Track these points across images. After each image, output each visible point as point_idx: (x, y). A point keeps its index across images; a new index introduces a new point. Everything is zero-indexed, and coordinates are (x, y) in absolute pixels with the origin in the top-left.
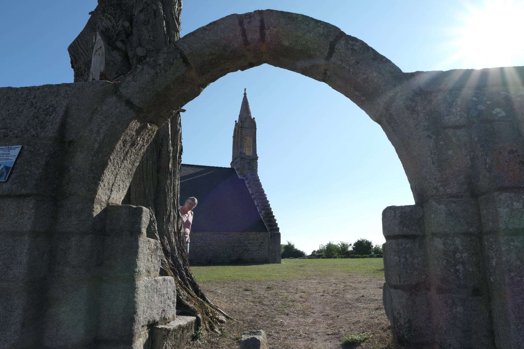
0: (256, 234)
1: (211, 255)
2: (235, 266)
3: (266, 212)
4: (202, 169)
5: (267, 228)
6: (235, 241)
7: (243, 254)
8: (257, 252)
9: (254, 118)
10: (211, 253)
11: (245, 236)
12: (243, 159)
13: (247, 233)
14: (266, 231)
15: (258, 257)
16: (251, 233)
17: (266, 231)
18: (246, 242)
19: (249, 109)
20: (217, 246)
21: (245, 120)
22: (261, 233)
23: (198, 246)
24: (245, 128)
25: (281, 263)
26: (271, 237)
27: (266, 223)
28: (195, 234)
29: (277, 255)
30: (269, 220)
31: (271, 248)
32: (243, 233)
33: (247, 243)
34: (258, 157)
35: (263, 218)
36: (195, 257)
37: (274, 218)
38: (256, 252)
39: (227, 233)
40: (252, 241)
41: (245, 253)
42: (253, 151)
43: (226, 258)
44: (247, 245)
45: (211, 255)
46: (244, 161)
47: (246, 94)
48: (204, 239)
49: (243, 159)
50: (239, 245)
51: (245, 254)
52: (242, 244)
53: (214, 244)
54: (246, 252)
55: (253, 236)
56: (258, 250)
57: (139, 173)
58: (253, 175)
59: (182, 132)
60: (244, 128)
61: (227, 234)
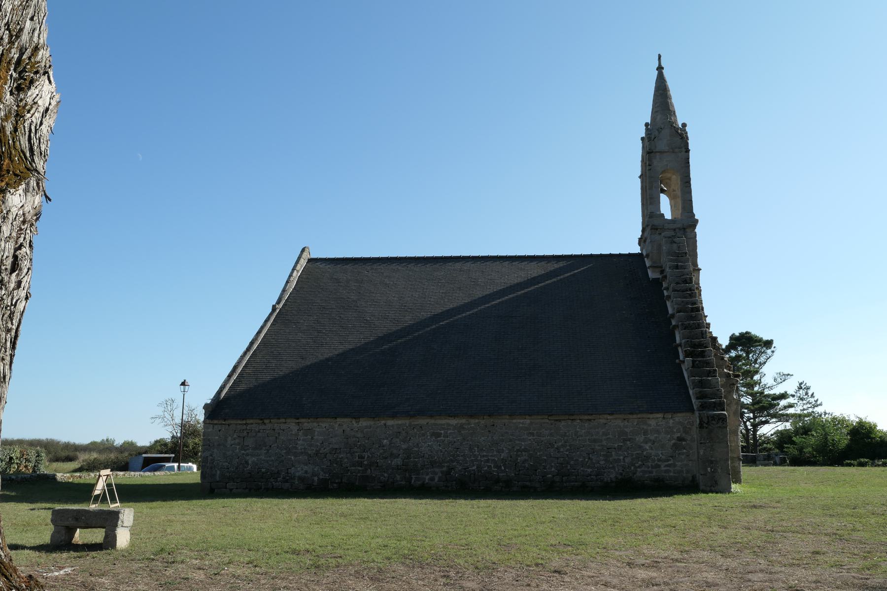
0: (664, 418)
1: (553, 469)
2: (415, 498)
3: (696, 361)
4: (562, 264)
5: (693, 401)
6: (610, 436)
7: (632, 468)
8: (670, 462)
9: (684, 125)
10: (553, 464)
11: (635, 424)
12: (657, 229)
13: (639, 416)
14: (692, 410)
15: (671, 474)
16: (651, 416)
17: (692, 410)
18: (640, 439)
19: (671, 103)
20: (568, 447)
21: (659, 132)
22: (679, 415)
23: (523, 447)
25: (730, 492)
26: (701, 426)
27: (694, 388)
28: (514, 421)
29: (719, 470)
30: (700, 381)
31: (702, 453)
32: (631, 416)
34: (697, 221)
35: (688, 376)
36: (515, 474)
38: (667, 463)
39: (590, 417)
40: (655, 435)
41: (637, 465)
42: (684, 208)
43: (590, 475)
44: (642, 444)
45: (553, 469)
46: (660, 234)
47: (663, 68)
48: (535, 432)
50: (621, 446)
51: (639, 467)
52: (628, 442)
53: (560, 444)
54: (640, 463)
55: (657, 423)
56: (672, 457)
58: (677, 267)
59: (25, 311)
60: (656, 152)
61: (590, 420)
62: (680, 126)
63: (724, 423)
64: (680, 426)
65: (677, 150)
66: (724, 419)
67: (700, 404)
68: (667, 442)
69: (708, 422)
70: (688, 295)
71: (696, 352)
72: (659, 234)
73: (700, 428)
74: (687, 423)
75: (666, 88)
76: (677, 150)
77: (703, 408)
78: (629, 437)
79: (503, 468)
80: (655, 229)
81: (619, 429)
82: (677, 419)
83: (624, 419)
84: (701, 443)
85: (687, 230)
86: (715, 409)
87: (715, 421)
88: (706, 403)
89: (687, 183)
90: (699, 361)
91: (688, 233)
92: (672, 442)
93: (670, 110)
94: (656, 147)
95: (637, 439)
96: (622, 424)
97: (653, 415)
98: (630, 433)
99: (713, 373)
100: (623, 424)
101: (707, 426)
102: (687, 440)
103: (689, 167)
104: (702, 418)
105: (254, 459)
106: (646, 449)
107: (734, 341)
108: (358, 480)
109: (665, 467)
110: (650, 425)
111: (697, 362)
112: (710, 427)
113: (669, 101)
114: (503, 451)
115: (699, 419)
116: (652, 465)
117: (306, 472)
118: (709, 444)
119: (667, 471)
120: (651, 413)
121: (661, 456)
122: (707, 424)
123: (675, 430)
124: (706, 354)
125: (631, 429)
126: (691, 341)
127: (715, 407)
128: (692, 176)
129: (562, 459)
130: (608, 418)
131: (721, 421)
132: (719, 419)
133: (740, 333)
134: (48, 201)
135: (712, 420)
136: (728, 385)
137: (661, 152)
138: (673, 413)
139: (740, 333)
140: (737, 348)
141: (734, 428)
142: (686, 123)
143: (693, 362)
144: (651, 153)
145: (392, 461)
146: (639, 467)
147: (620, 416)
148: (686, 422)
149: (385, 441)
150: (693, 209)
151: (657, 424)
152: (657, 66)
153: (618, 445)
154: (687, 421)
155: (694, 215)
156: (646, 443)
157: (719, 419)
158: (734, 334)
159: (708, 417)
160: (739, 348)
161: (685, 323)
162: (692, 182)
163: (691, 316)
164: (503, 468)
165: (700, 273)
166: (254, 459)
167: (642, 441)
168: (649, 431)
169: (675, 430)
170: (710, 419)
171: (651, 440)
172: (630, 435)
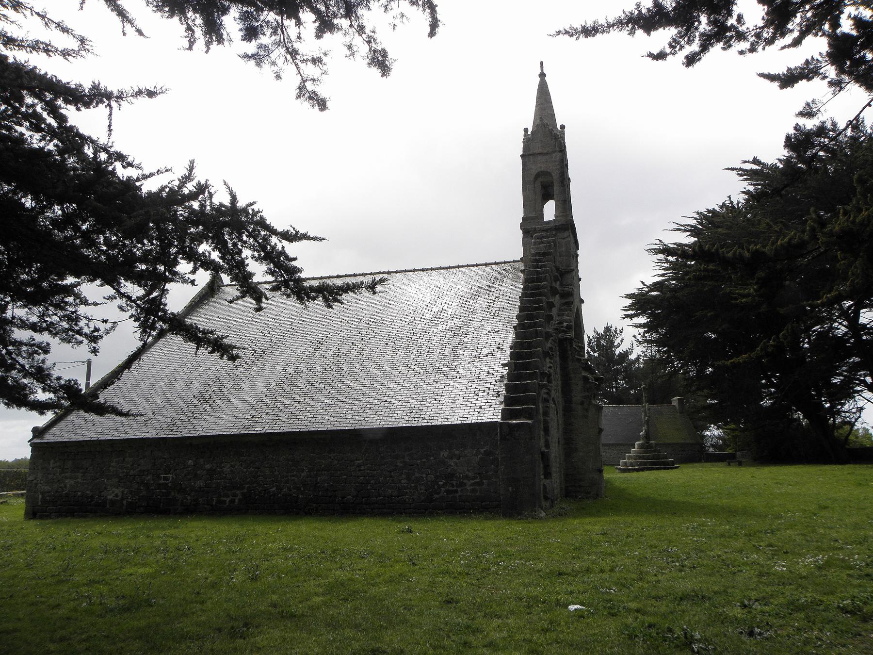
9: (563, 127)
62: (559, 128)
71: (533, 343)
79: (302, 489)
92: (479, 457)
105: (72, 482)
106: (451, 466)
108: (541, 411)
109: (470, 486)
114: (303, 471)
116: (457, 483)
117: (116, 496)
119: (474, 491)
121: (467, 473)
129: (362, 478)
134: (386, 283)
145: (195, 484)
146: (443, 486)
149: (190, 461)
156: (451, 458)
164: (302, 489)
166: (72, 482)
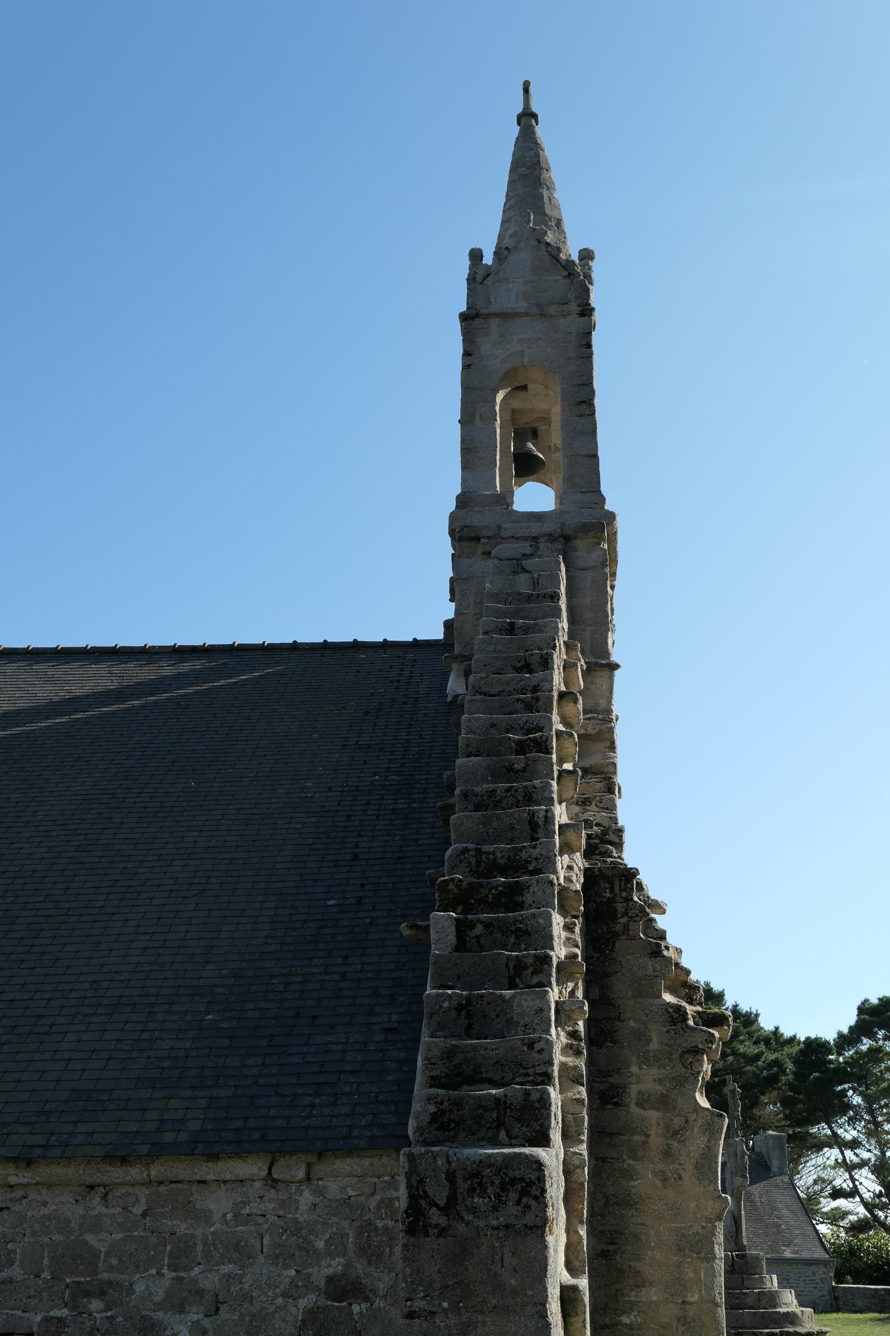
5: (420, 1078)
9: (587, 255)
11: (138, 1210)
13: (156, 1170)
16: (209, 1171)
22: (342, 1164)
24: (496, 315)
32: (116, 1173)
33: (159, 1294)
37: (603, 508)
40: (227, 1268)
44: (160, 1315)
47: (535, 116)
49: (478, 539)
50: (61, 1321)
52: (95, 1305)
57: (407, 777)
60: (490, 315)
63: (527, 1207)
64: (346, 1224)
65: (553, 310)
66: (530, 1184)
67: (432, 1109)
68: (280, 1301)
69: (452, 1199)
70: (520, 706)
71: (485, 891)
72: (484, 553)
73: (411, 1231)
74: (378, 1207)
75: (539, 162)
76: (553, 310)
77: (444, 1128)
78: (105, 1276)
80: (470, 539)
81: (60, 1238)
82: (333, 1188)
83: (91, 1187)
84: (411, 1315)
85: (578, 543)
86: (503, 1135)
87: (483, 1193)
88: (458, 1104)
89: (584, 406)
90: (487, 925)
91: (578, 554)
93: (546, 215)
94: (489, 301)
95: (139, 1288)
96: (74, 1212)
97: (221, 1164)
98: (108, 1253)
99: (535, 973)
100: (80, 1210)
101: (443, 1221)
102: (374, 1291)
103: (589, 357)
104: (421, 1182)
107: (867, 1017)
110: (206, 1218)
111: (479, 929)
112: (461, 1228)
113: (545, 193)
115: (409, 1187)
118: (453, 1320)
120: (214, 1157)
122: (444, 1210)
123: (320, 1244)
124: (528, 897)
125: (118, 1236)
126: (478, 850)
127: (500, 1124)
128: (597, 384)
130: (12, 1180)
131: (513, 1195)
132: (504, 1187)
133: (879, 999)
135: (472, 1190)
136: (676, 1056)
137: (505, 316)
138: (312, 1159)
139: (879, 999)
140: (876, 1033)
141: (696, 1228)
142: (591, 247)
143: (462, 927)
144: (473, 318)
147: (57, 1171)
148: (373, 1202)
150: (599, 483)
151: (237, 1215)
152: (520, 109)
153: (46, 1319)
154: (377, 1198)
155: (603, 500)
157: (504, 1187)
158: (866, 1001)
159: (451, 1177)
160: (881, 1034)
161: (478, 789)
162: (597, 402)
163: (510, 769)
165: (615, 679)
167: (158, 1298)
168: (200, 1248)
169: (320, 1244)
170: (463, 1186)
171: (200, 1293)
172: (111, 1268)
